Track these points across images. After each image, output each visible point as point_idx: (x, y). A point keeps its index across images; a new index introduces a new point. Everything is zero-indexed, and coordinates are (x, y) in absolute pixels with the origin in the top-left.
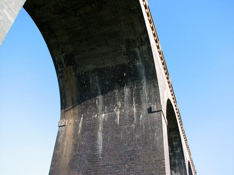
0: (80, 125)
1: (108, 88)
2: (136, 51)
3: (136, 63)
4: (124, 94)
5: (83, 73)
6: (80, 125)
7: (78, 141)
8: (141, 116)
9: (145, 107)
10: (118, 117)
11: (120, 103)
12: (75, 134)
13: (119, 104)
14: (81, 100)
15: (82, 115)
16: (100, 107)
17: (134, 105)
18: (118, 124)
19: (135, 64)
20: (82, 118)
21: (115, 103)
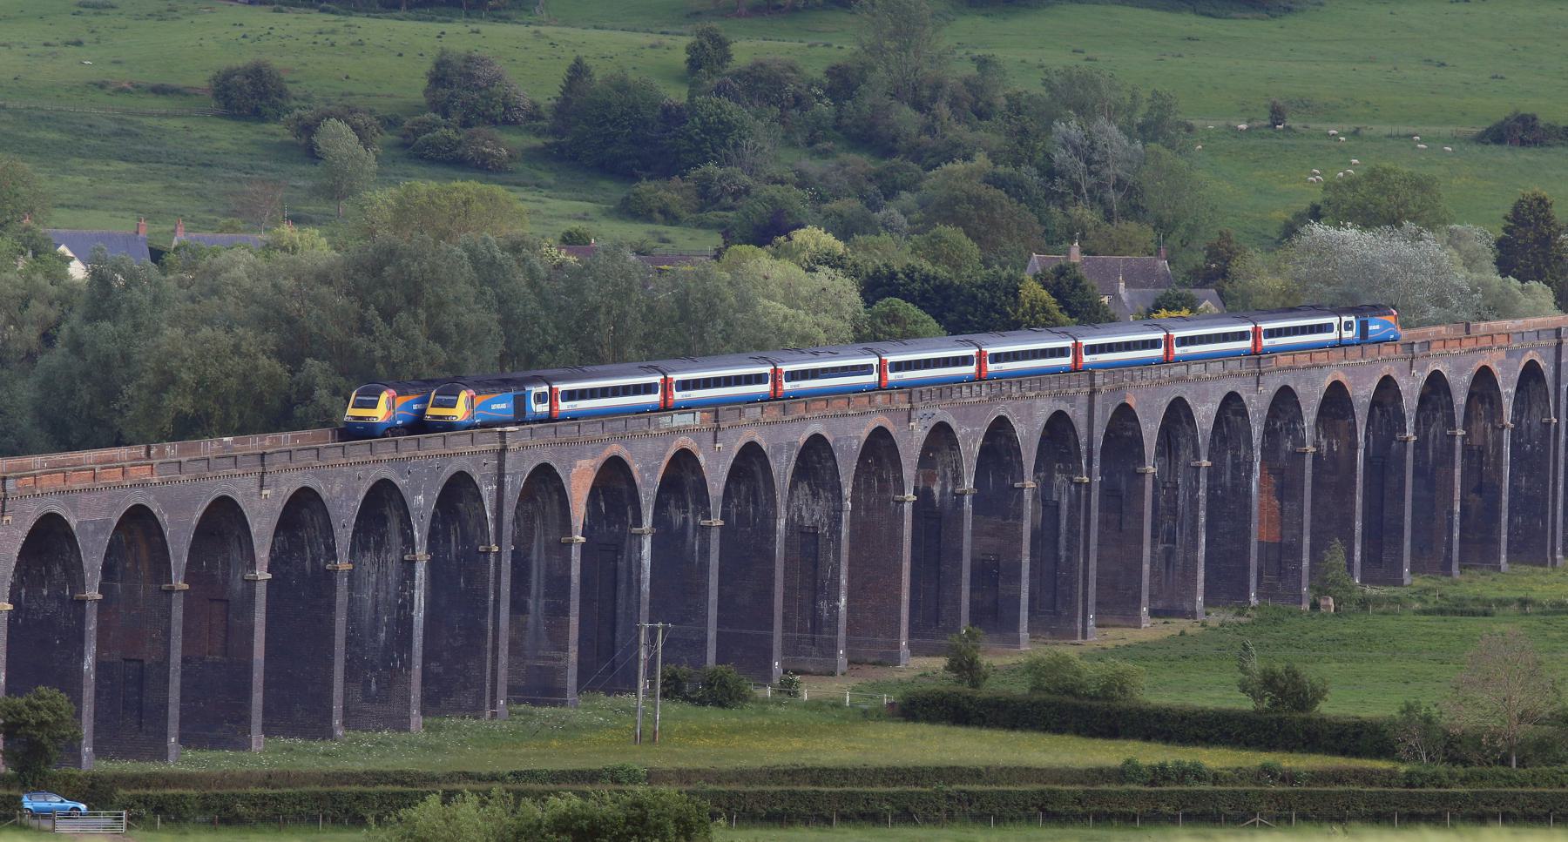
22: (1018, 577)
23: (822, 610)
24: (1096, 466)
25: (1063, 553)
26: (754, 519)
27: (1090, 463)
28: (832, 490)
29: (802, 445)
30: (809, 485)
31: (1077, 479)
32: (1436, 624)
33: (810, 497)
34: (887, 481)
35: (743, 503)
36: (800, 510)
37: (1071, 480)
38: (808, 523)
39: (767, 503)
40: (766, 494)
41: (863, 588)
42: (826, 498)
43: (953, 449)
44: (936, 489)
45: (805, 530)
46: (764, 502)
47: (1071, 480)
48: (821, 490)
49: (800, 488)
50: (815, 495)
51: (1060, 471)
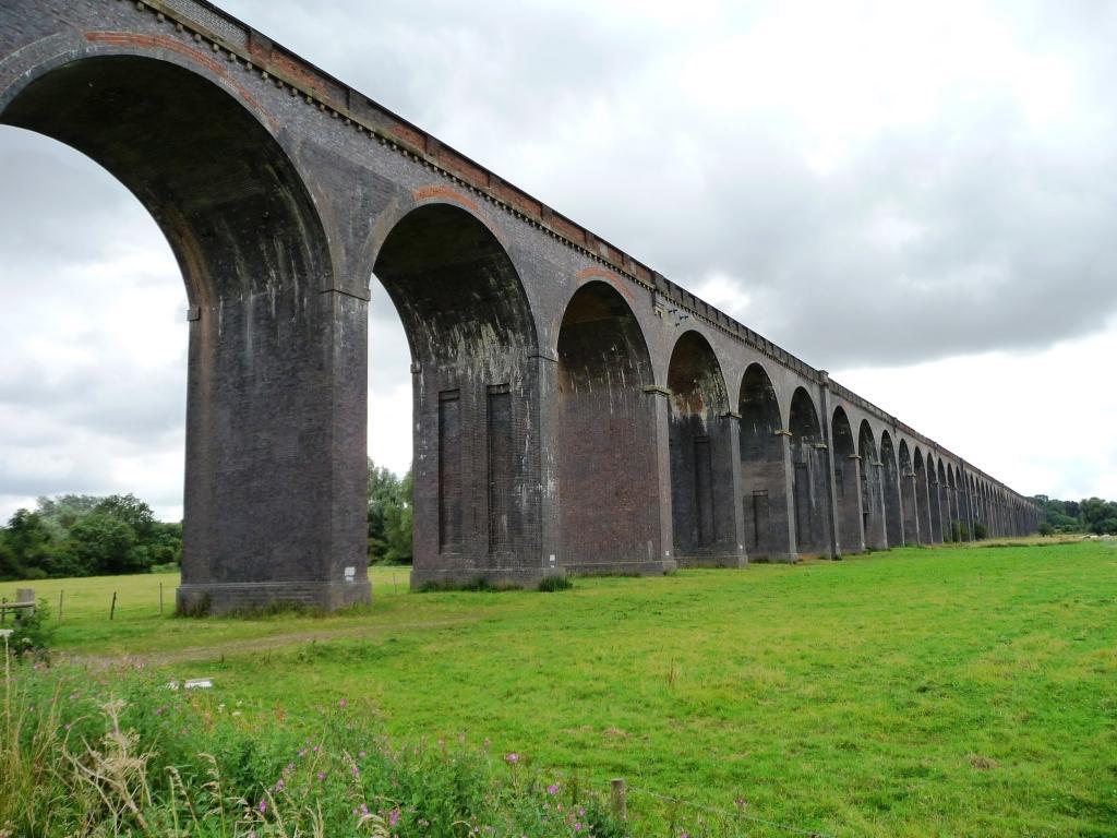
6: (220, 318)
13: (273, 273)
16: (245, 280)
22: (784, 507)
23: (521, 501)
24: (830, 438)
25: (813, 501)
26: (301, 301)
27: (826, 435)
28: (523, 327)
29: (417, 206)
30: (495, 328)
31: (819, 445)
32: (488, 624)
33: (497, 345)
34: (634, 371)
35: (284, 277)
36: (487, 365)
37: (814, 447)
38: (496, 381)
39: (317, 267)
40: (314, 247)
41: (617, 494)
42: (518, 341)
43: (716, 372)
44: (703, 415)
45: (495, 390)
46: (313, 263)
47: (814, 447)
48: (509, 332)
49: (484, 335)
50: (504, 340)
51: (805, 442)
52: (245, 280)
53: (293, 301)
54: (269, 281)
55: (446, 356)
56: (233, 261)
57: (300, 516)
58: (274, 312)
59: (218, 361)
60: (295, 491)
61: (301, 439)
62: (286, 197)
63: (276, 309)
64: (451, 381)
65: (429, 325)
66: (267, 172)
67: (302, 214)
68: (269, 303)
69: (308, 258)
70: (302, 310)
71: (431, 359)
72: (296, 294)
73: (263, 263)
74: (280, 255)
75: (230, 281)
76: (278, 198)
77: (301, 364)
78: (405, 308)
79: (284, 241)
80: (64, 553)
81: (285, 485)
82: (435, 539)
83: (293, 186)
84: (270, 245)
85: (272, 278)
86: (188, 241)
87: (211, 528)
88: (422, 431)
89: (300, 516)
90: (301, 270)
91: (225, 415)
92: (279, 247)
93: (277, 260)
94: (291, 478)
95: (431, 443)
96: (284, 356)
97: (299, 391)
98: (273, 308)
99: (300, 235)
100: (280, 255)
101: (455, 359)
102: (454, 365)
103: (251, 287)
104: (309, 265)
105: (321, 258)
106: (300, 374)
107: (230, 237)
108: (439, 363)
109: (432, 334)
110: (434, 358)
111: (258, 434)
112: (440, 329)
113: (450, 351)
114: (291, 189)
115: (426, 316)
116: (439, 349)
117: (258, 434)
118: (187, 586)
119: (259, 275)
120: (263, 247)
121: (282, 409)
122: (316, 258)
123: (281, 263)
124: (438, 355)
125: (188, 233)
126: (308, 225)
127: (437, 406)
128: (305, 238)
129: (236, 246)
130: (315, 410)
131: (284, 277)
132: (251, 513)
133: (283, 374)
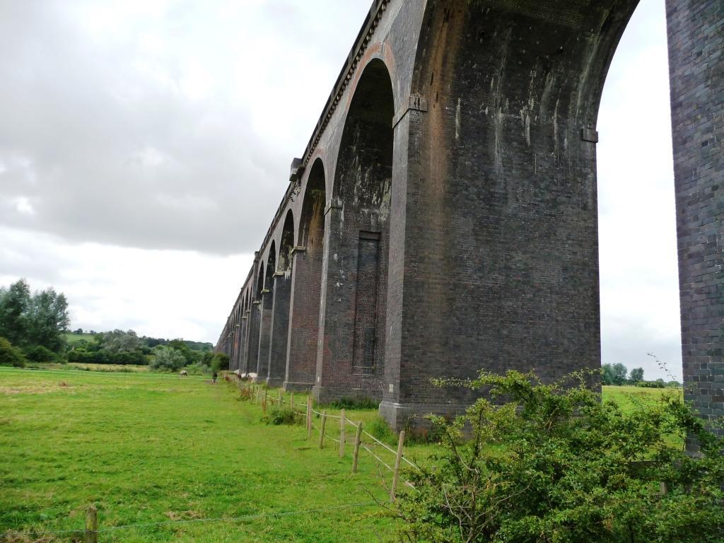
0: (457, 121)
1: (520, 63)
2: (602, 16)
3: (589, 36)
4: (543, 87)
5: (489, 9)
6: (457, 121)
7: (456, 155)
8: (566, 140)
9: (572, 122)
10: (528, 129)
11: (533, 101)
12: (448, 136)
13: (532, 102)
14: (462, 65)
15: (459, 100)
16: (496, 95)
17: (555, 115)
18: (566, 147)
19: (586, 38)
20: (459, 107)
21: (525, 98)
26: (561, 140)
40: (585, 98)
52: (496, 95)
53: (551, 137)
54: (525, 108)
55: (369, 201)
56: (491, 72)
57: (566, 342)
58: (528, 139)
59: (455, 165)
60: (559, 318)
61: (565, 269)
62: (592, 44)
63: (531, 134)
64: (372, 223)
65: (363, 171)
66: (599, 15)
67: (593, 66)
68: (523, 129)
69: (575, 105)
70: (562, 148)
71: (353, 200)
72: (555, 132)
73: (525, 89)
74: (548, 89)
75: (478, 88)
76: (583, 41)
77: (564, 199)
78: (350, 150)
79: (558, 79)
80: (28, 365)
81: (548, 310)
82: (349, 359)
83: (608, 39)
84: (542, 75)
85: (529, 107)
86: (450, 28)
87: (446, 344)
88: (339, 260)
89: (566, 342)
90: (564, 111)
91: (465, 225)
92: (551, 82)
93: (542, 93)
94: (554, 305)
95: (349, 274)
96: (542, 185)
97: (562, 224)
98: (528, 135)
99: (578, 82)
100: (548, 89)
101: (379, 206)
102: (377, 211)
103: (501, 105)
104: (574, 112)
105: (588, 109)
106: (562, 208)
107: (504, 48)
108: (361, 206)
109: (363, 179)
110: (356, 200)
111: (513, 254)
112: (372, 173)
113: (375, 198)
114: (603, 40)
115: (365, 162)
116: (363, 194)
117: (513, 254)
118: (409, 407)
119: (516, 95)
120: (533, 74)
121: (540, 236)
122: (583, 107)
123: (544, 96)
124: (361, 198)
125: (458, 21)
126: (591, 76)
127: (357, 242)
128: (581, 86)
129: (504, 60)
130: (580, 245)
131: (542, 110)
132: (505, 332)
133: (542, 201)
